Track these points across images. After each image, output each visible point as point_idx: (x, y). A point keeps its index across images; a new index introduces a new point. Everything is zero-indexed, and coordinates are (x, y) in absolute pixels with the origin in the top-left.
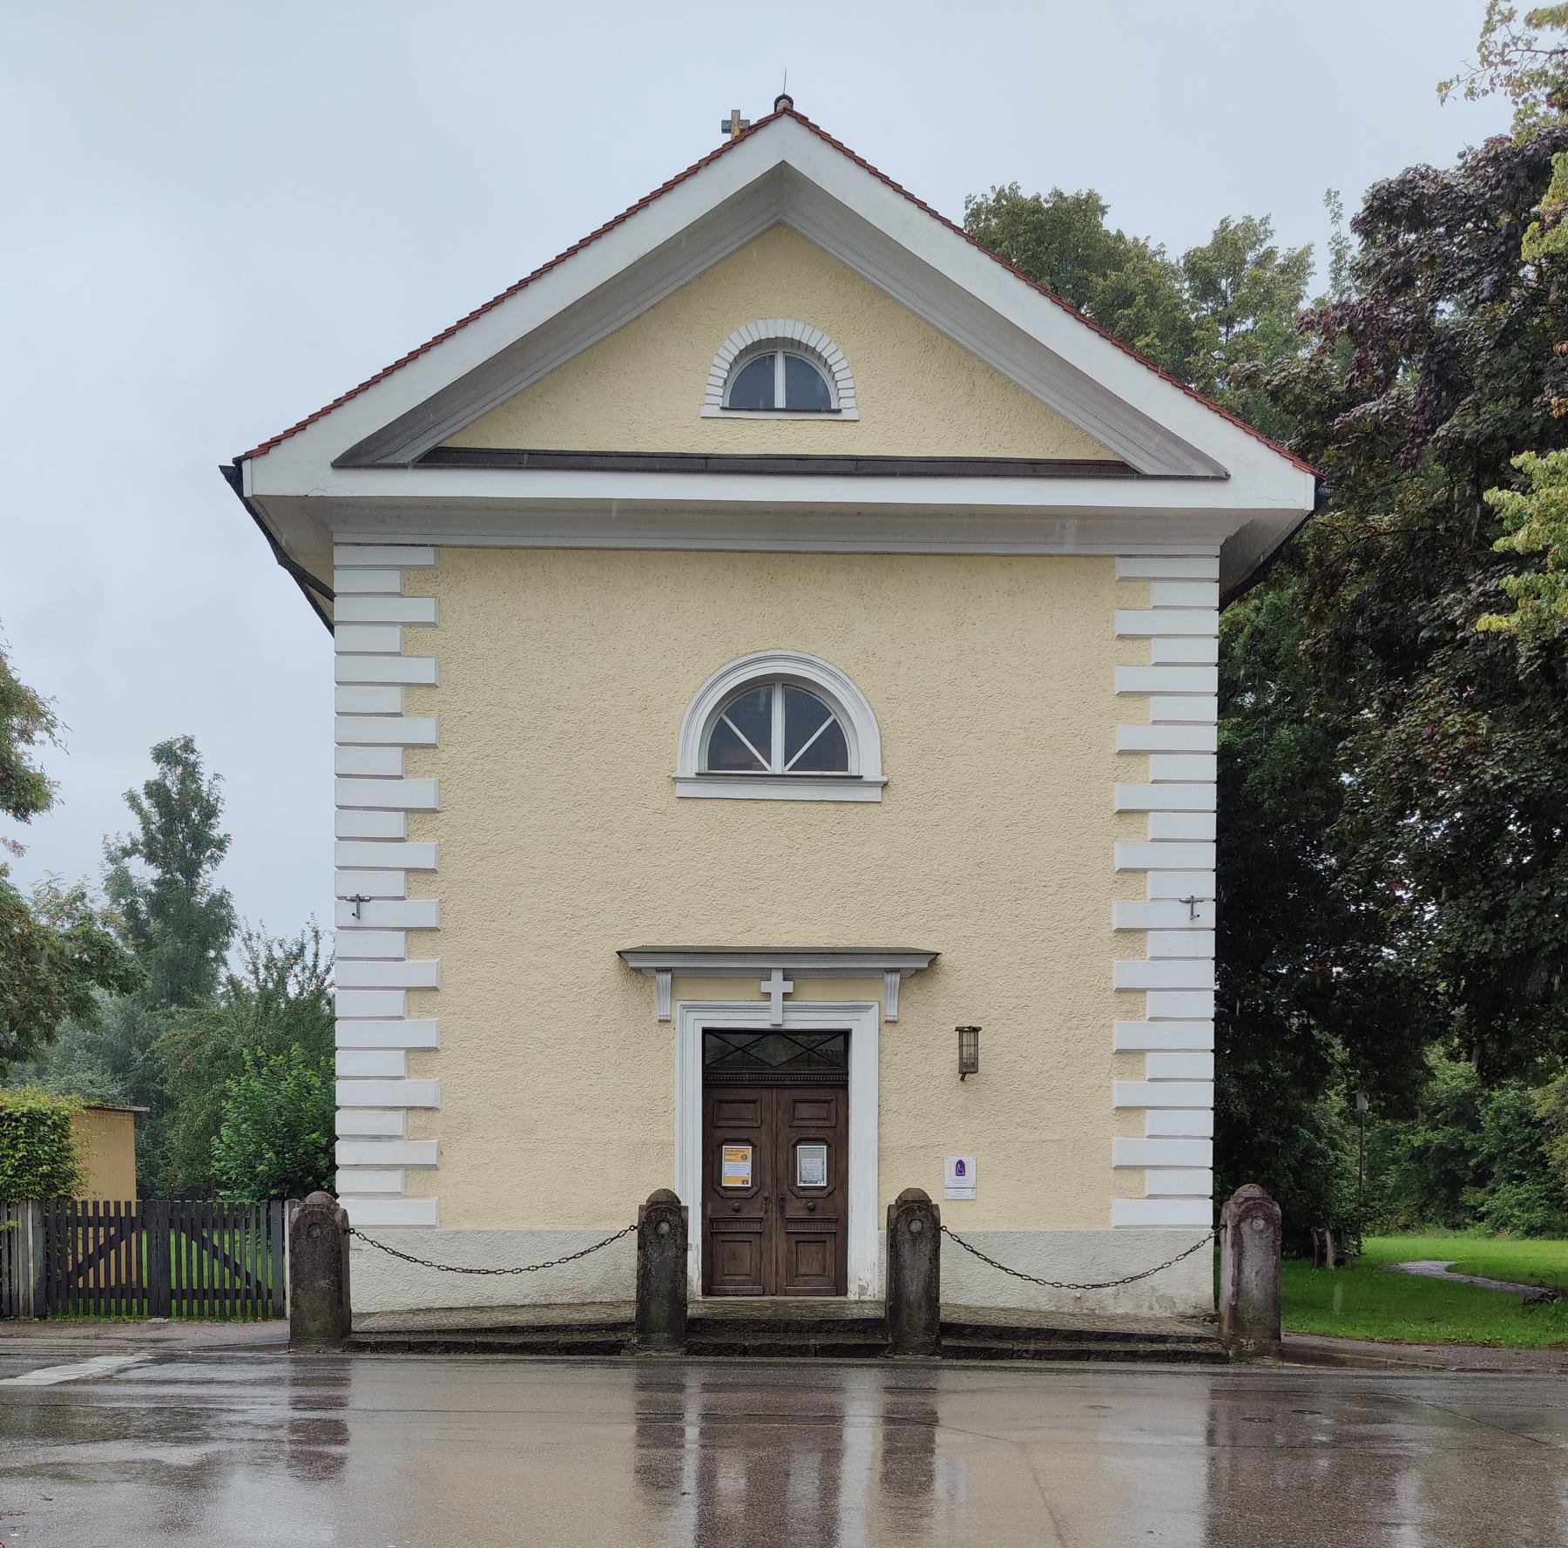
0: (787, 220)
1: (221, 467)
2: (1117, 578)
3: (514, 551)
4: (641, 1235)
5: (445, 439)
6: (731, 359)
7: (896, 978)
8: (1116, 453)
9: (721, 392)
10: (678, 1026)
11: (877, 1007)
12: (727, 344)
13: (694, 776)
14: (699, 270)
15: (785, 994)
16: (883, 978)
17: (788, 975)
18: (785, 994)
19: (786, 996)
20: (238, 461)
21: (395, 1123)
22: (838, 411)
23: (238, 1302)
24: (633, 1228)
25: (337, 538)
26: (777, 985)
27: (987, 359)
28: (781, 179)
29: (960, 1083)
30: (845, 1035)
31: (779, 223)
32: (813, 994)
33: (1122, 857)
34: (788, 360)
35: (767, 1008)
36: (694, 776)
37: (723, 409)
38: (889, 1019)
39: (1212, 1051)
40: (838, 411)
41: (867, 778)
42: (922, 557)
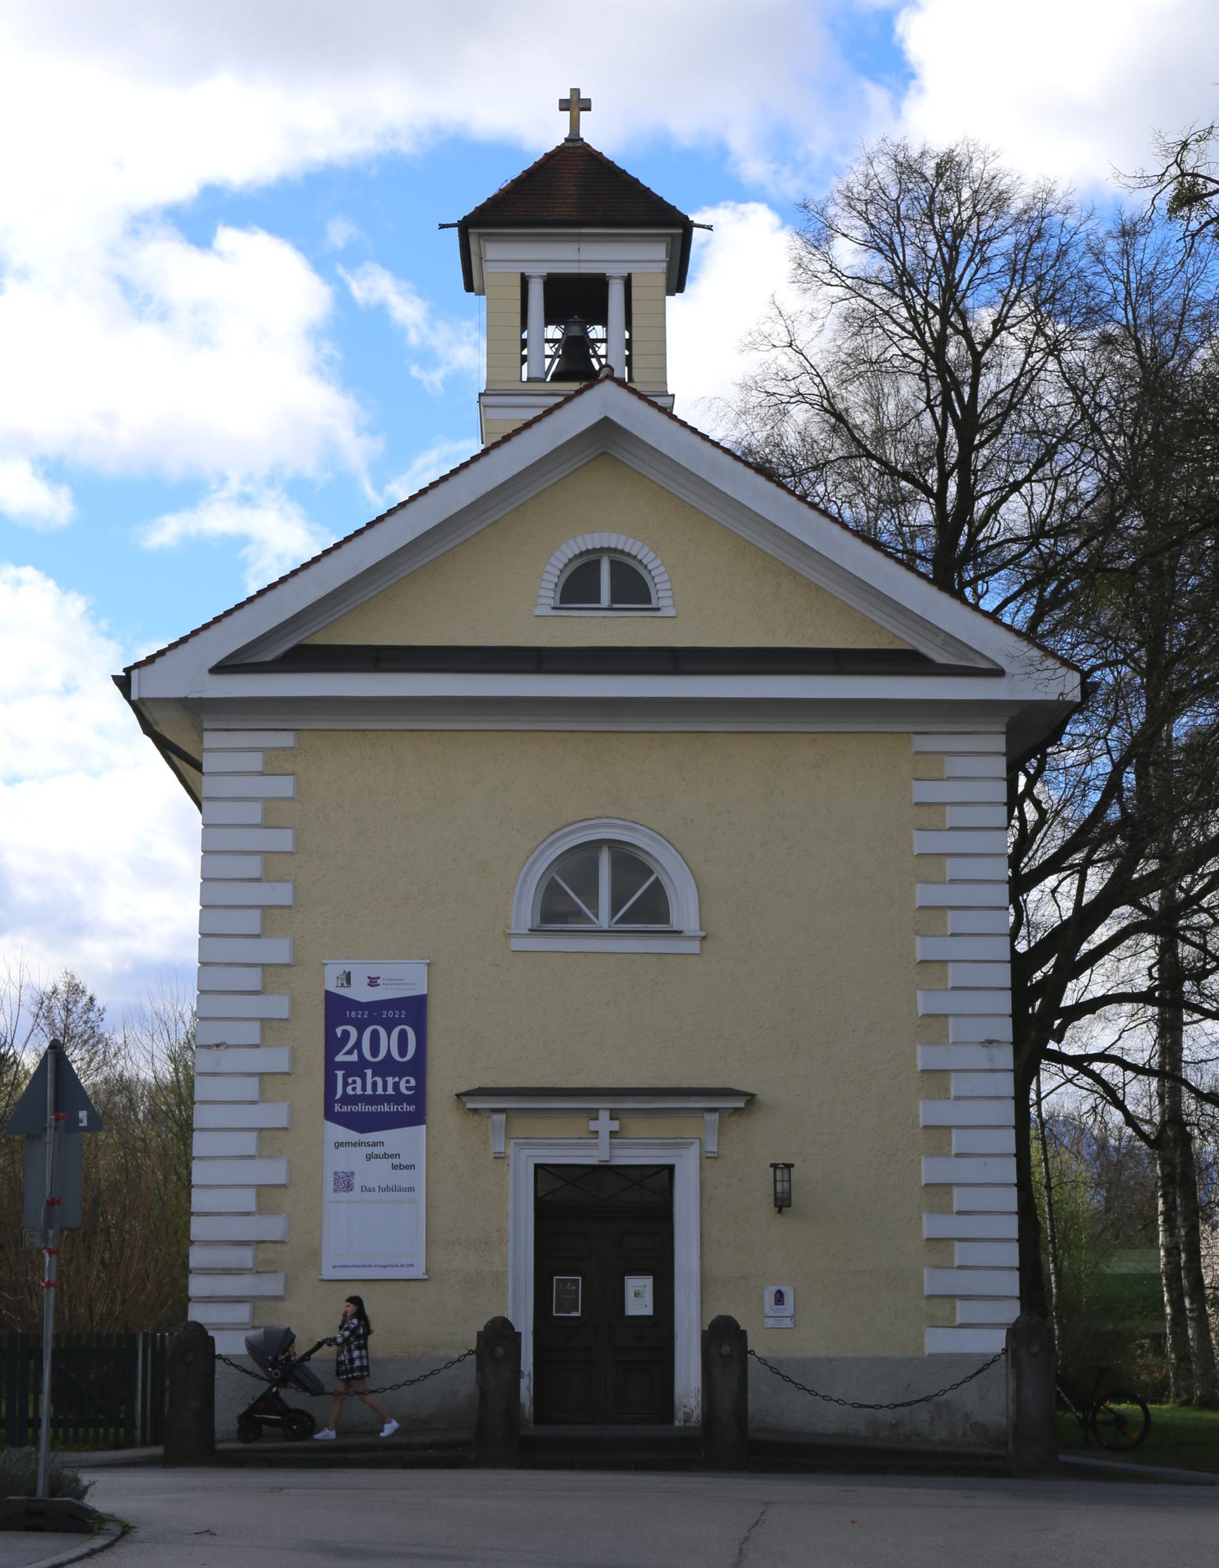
0: (609, 451)
1: (113, 676)
2: (913, 752)
3: (365, 733)
4: (480, 1359)
5: (306, 638)
6: (561, 566)
7: (716, 1116)
8: (910, 645)
9: (552, 594)
10: (511, 1162)
11: (697, 1142)
12: (558, 554)
13: (527, 932)
14: (534, 493)
15: (611, 1132)
16: (703, 1117)
17: (614, 1115)
18: (611, 1132)
19: (613, 1134)
20: (128, 670)
21: (245, 1257)
22: (658, 609)
23: (102, 1431)
24: (471, 1352)
25: (206, 725)
26: (604, 1124)
27: (788, 564)
28: (605, 427)
29: (778, 1215)
30: (670, 1169)
31: (604, 453)
32: (639, 1128)
33: (924, 1003)
34: (613, 563)
35: (596, 1145)
36: (527, 932)
37: (554, 608)
38: (709, 1155)
39: (1016, 1185)
40: (658, 609)
41: (687, 933)
42: (734, 735)
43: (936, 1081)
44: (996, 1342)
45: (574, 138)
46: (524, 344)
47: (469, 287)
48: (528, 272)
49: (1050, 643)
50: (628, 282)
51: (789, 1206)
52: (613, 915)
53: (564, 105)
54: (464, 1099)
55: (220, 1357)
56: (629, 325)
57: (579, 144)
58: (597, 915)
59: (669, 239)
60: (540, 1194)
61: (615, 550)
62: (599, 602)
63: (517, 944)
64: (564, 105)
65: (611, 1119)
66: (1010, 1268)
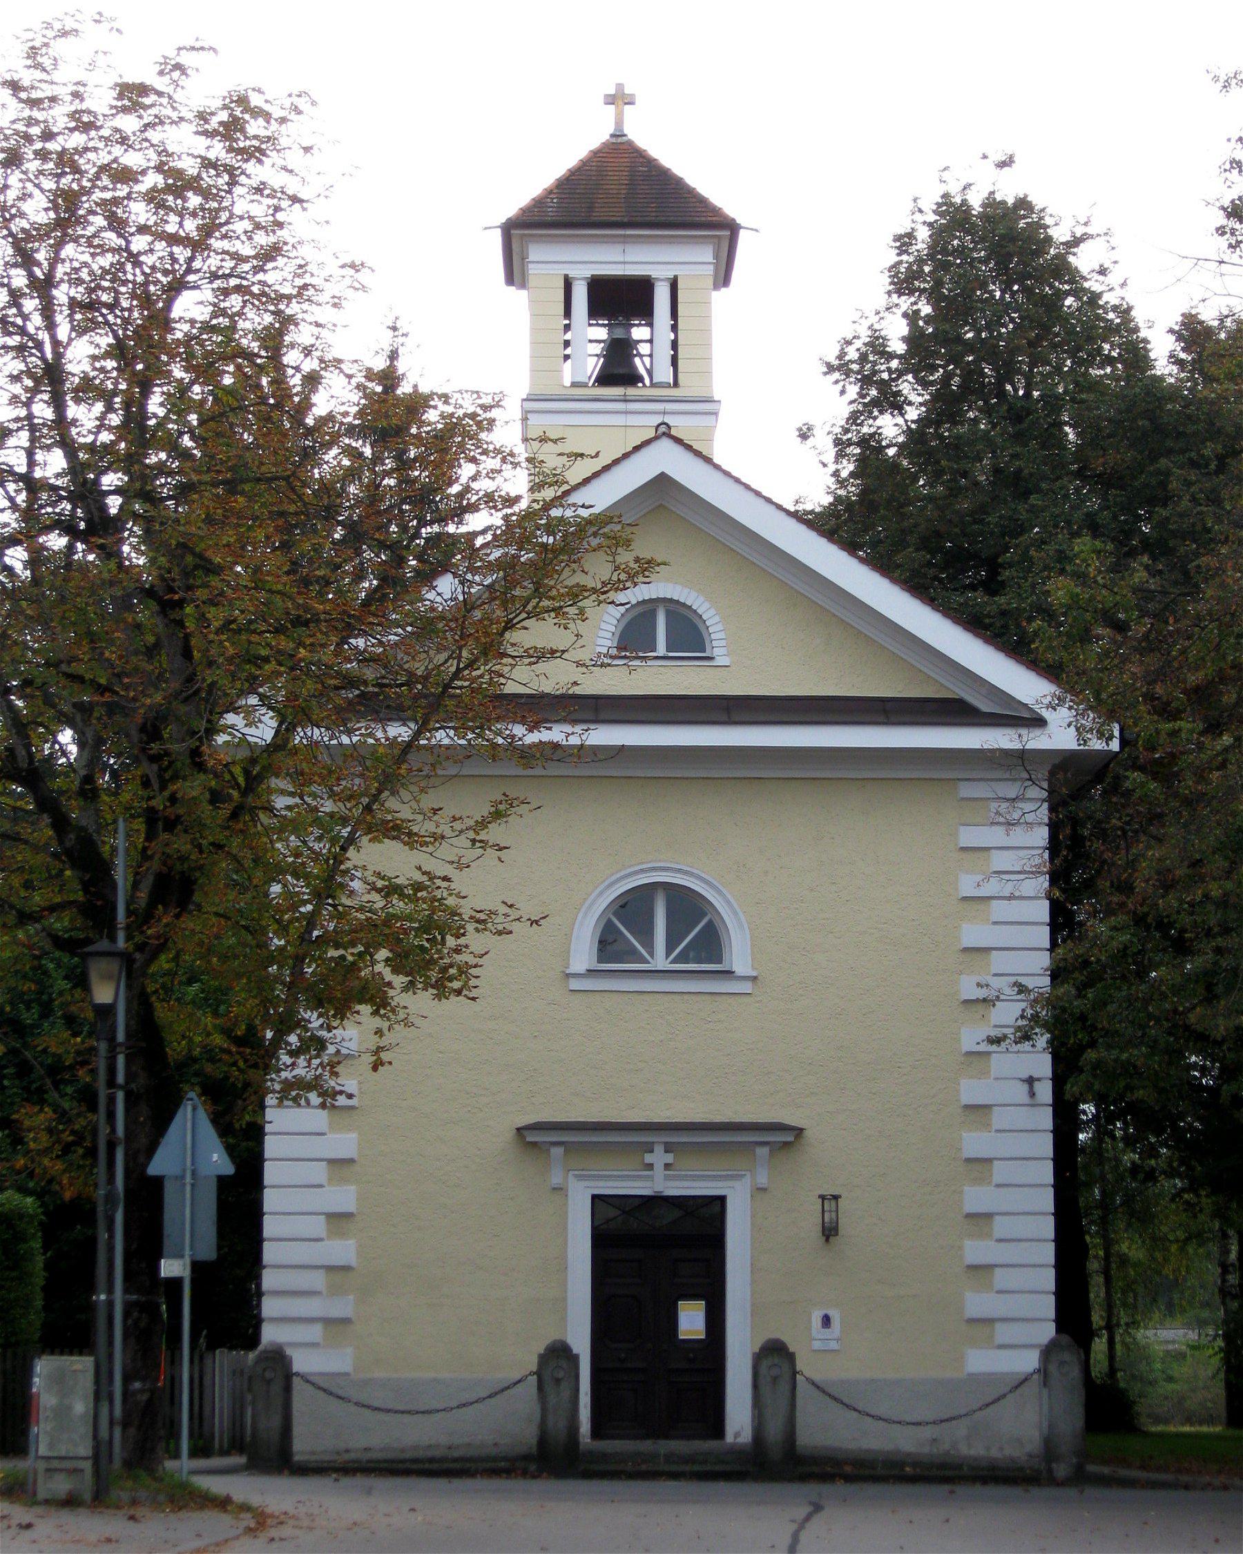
16: (754, 1151)
19: (667, 1166)
28: (663, 482)
30: (722, 1200)
31: (661, 505)
34: (669, 614)
43: (980, 1112)
44: (1029, 1361)
45: (618, 135)
46: (567, 344)
47: (510, 279)
48: (572, 274)
49: (1228, 1300)
50: (674, 285)
51: (837, 1234)
52: (668, 956)
53: (611, 100)
54: (525, 1133)
55: (297, 1374)
56: (674, 328)
57: (624, 139)
58: (652, 954)
59: (716, 240)
60: (596, 1224)
61: (671, 600)
62: (654, 650)
63: (575, 984)
64: (611, 100)
65: (666, 1152)
66: (1048, 1293)
